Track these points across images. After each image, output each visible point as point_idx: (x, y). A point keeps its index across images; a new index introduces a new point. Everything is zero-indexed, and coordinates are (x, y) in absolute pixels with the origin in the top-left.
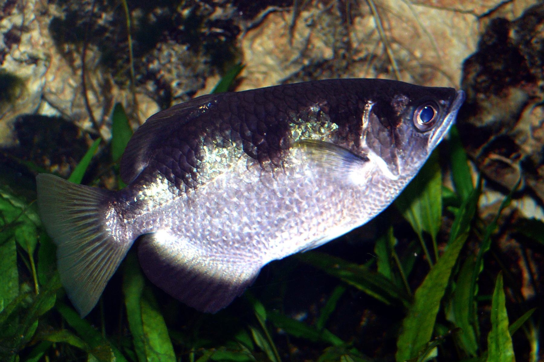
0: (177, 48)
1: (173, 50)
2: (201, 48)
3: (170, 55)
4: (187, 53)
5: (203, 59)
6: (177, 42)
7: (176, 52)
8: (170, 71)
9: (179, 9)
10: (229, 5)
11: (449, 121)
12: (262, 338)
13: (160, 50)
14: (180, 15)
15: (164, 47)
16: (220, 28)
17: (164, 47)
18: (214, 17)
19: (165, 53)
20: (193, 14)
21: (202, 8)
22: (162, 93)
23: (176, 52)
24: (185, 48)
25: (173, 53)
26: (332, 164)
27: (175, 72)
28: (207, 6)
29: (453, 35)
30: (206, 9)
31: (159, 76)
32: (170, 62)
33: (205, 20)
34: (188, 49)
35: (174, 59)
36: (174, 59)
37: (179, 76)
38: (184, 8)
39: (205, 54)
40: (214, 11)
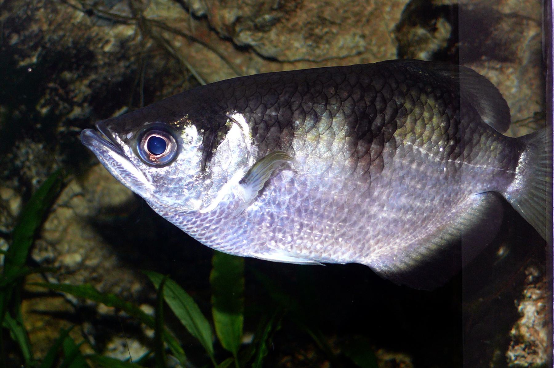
0: (33, 146)
1: (30, 147)
2: (58, 147)
3: (27, 153)
4: (43, 151)
5: (58, 158)
6: (34, 140)
7: (33, 150)
8: (29, 168)
9: (38, 108)
10: (86, 105)
11: (175, 297)
12: (199, 338)
13: (18, 148)
14: (39, 113)
15: (21, 145)
16: (78, 127)
17: (21, 145)
18: (72, 116)
19: (23, 151)
20: (51, 111)
21: (61, 107)
22: (24, 189)
23: (33, 150)
24: (41, 146)
25: (30, 151)
26: (514, 19)
27: (34, 170)
28: (66, 105)
29: (167, 185)
30: (65, 108)
31: (22, 173)
32: (28, 159)
33: (64, 119)
34: (44, 148)
35: (31, 157)
36: (31, 157)
37: (38, 174)
38: (43, 106)
39: (61, 154)
40: (72, 110)
